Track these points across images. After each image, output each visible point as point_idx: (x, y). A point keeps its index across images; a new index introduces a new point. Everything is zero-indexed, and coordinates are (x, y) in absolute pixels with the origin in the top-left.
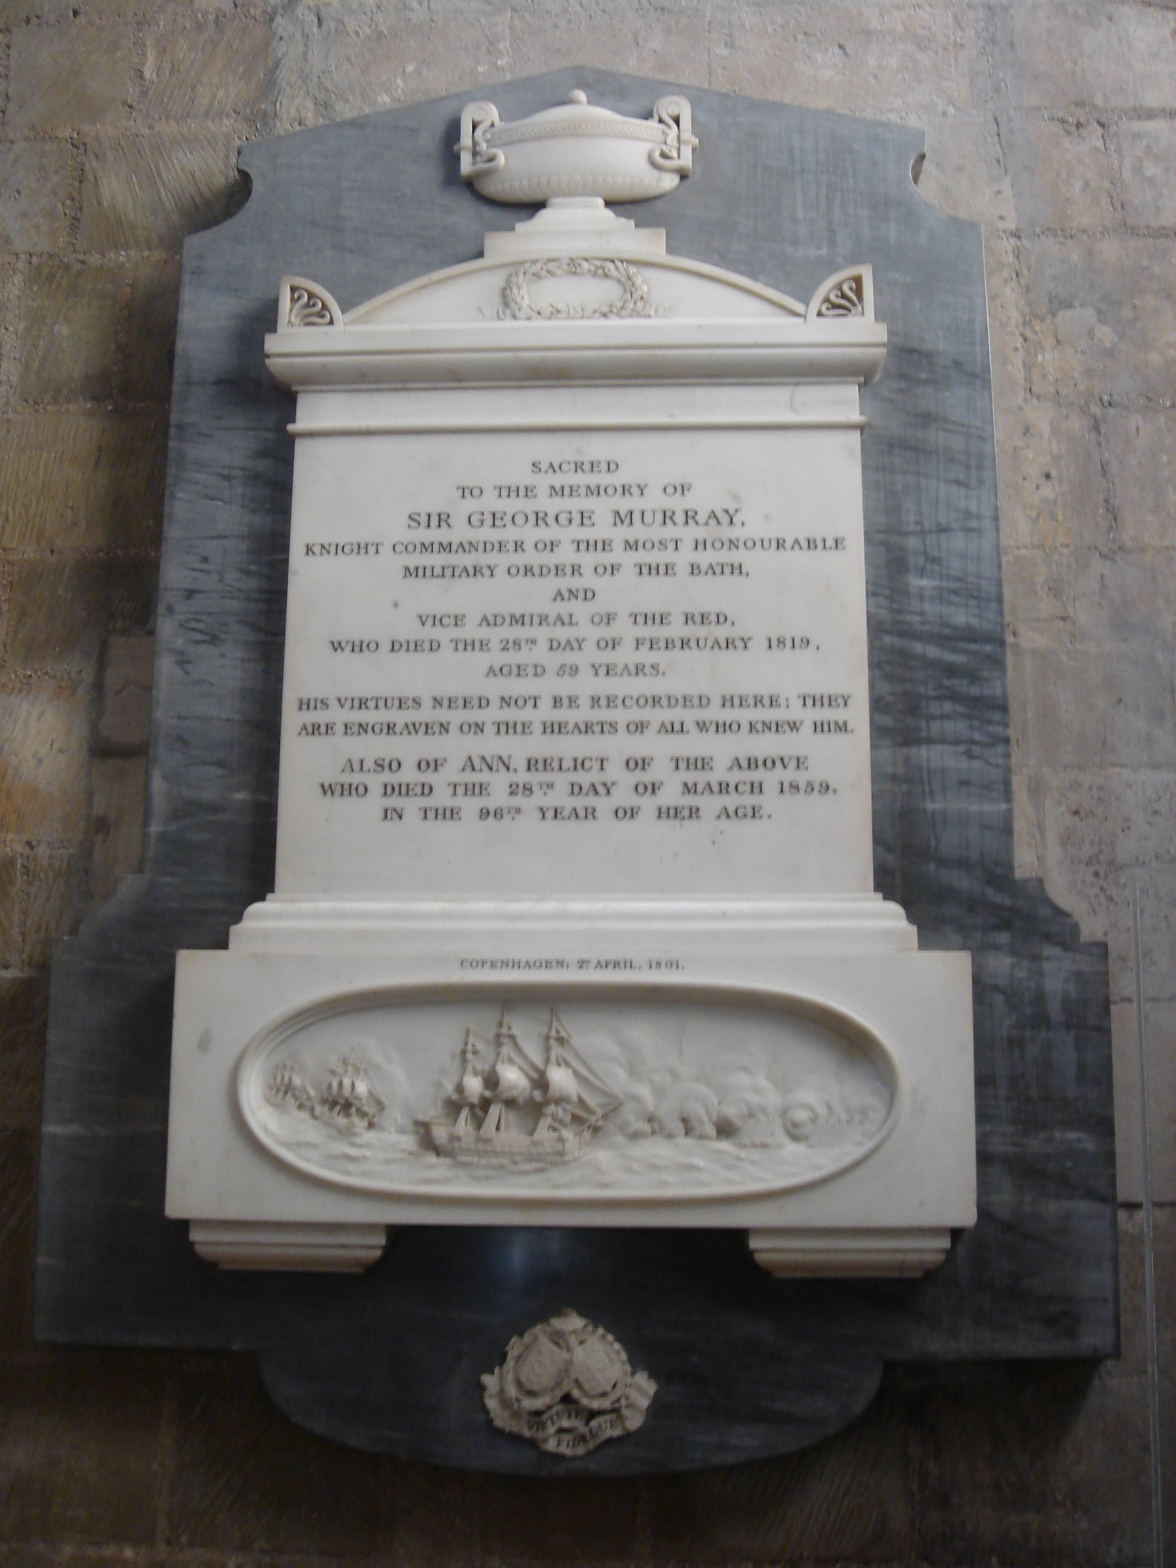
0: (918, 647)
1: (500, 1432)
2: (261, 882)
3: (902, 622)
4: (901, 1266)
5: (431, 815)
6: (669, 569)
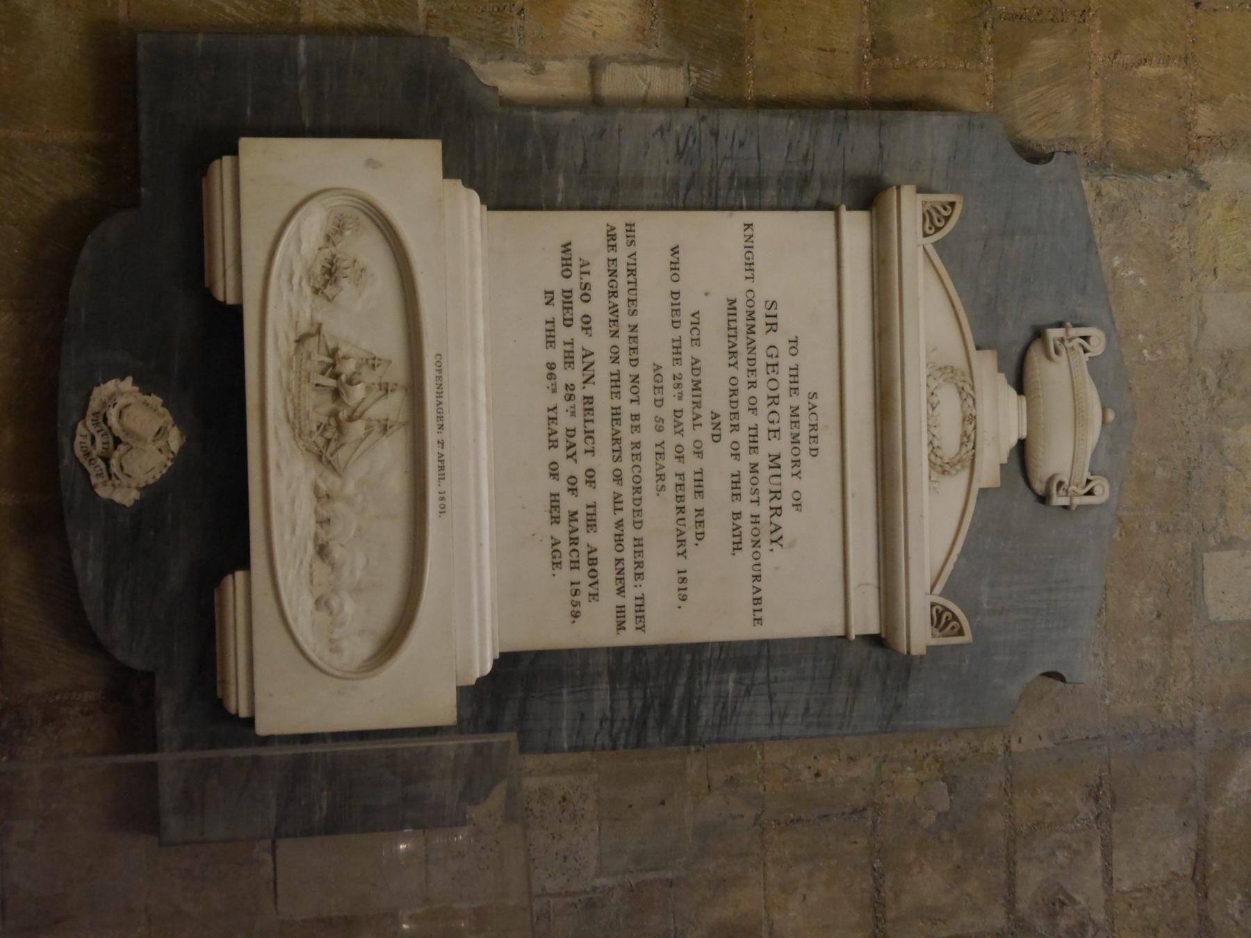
0: (683, 680)
1: (90, 393)
2: (494, 203)
3: (701, 669)
4: (224, 682)
5: (549, 326)
6: (736, 496)
